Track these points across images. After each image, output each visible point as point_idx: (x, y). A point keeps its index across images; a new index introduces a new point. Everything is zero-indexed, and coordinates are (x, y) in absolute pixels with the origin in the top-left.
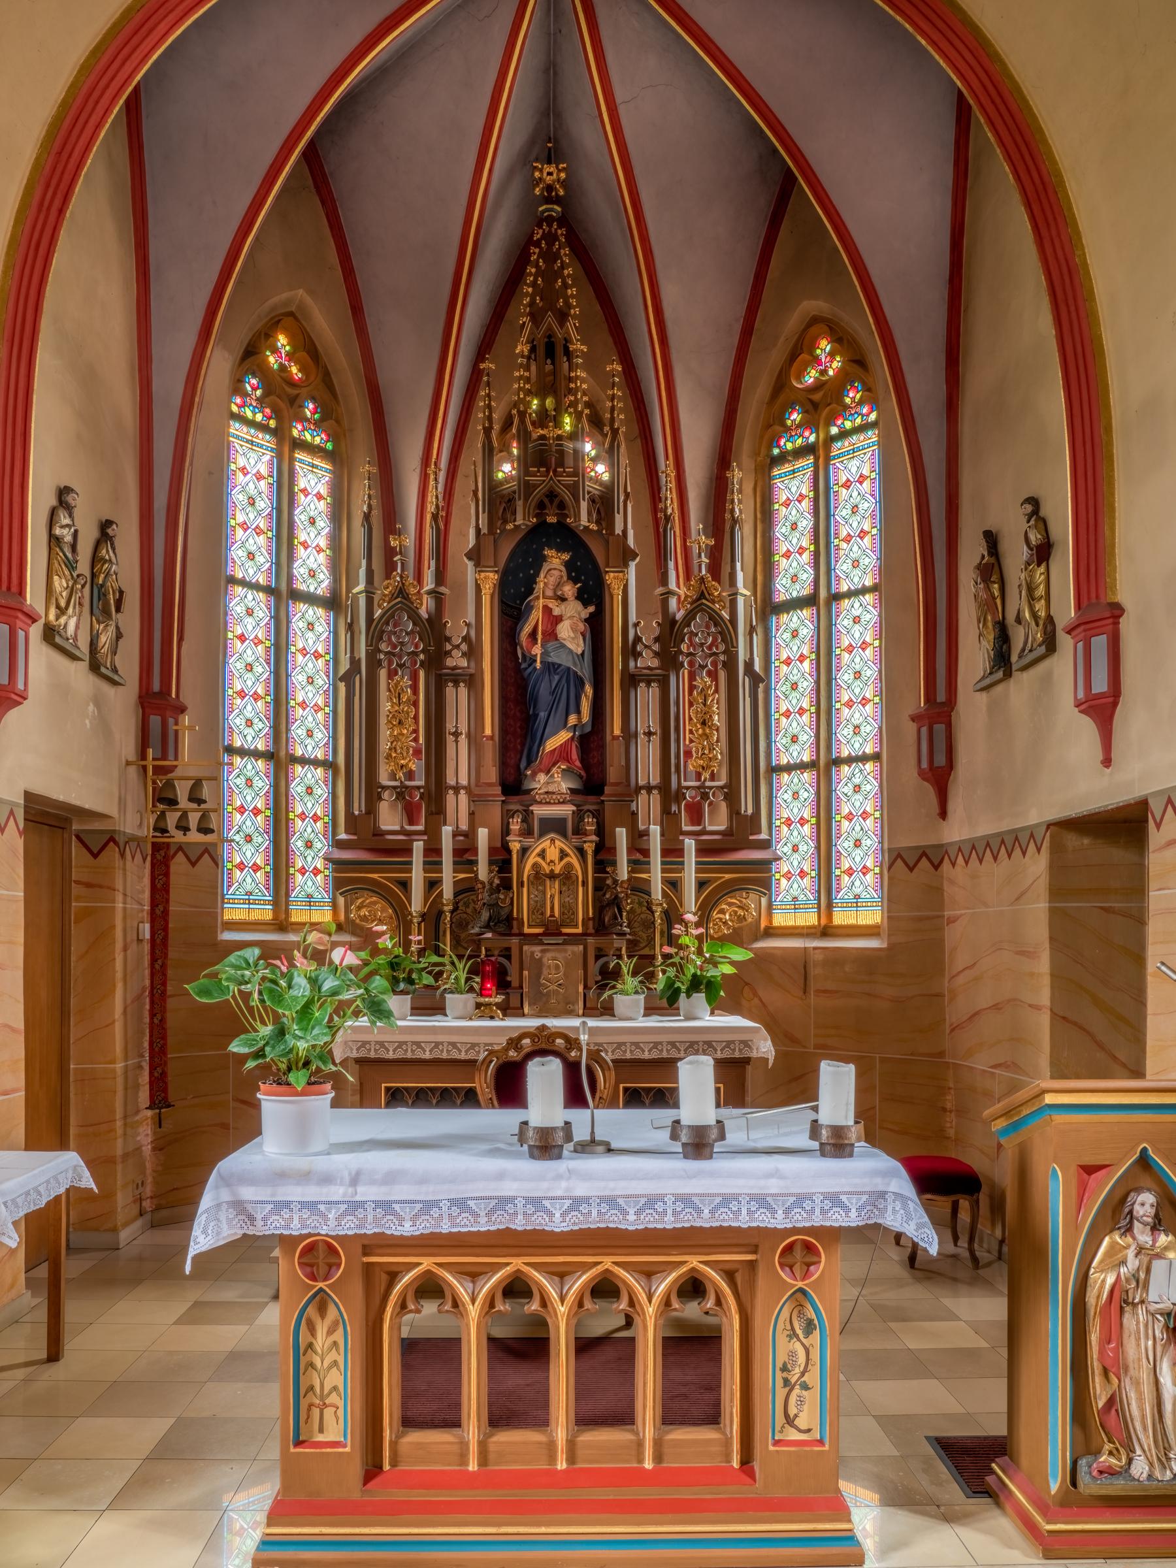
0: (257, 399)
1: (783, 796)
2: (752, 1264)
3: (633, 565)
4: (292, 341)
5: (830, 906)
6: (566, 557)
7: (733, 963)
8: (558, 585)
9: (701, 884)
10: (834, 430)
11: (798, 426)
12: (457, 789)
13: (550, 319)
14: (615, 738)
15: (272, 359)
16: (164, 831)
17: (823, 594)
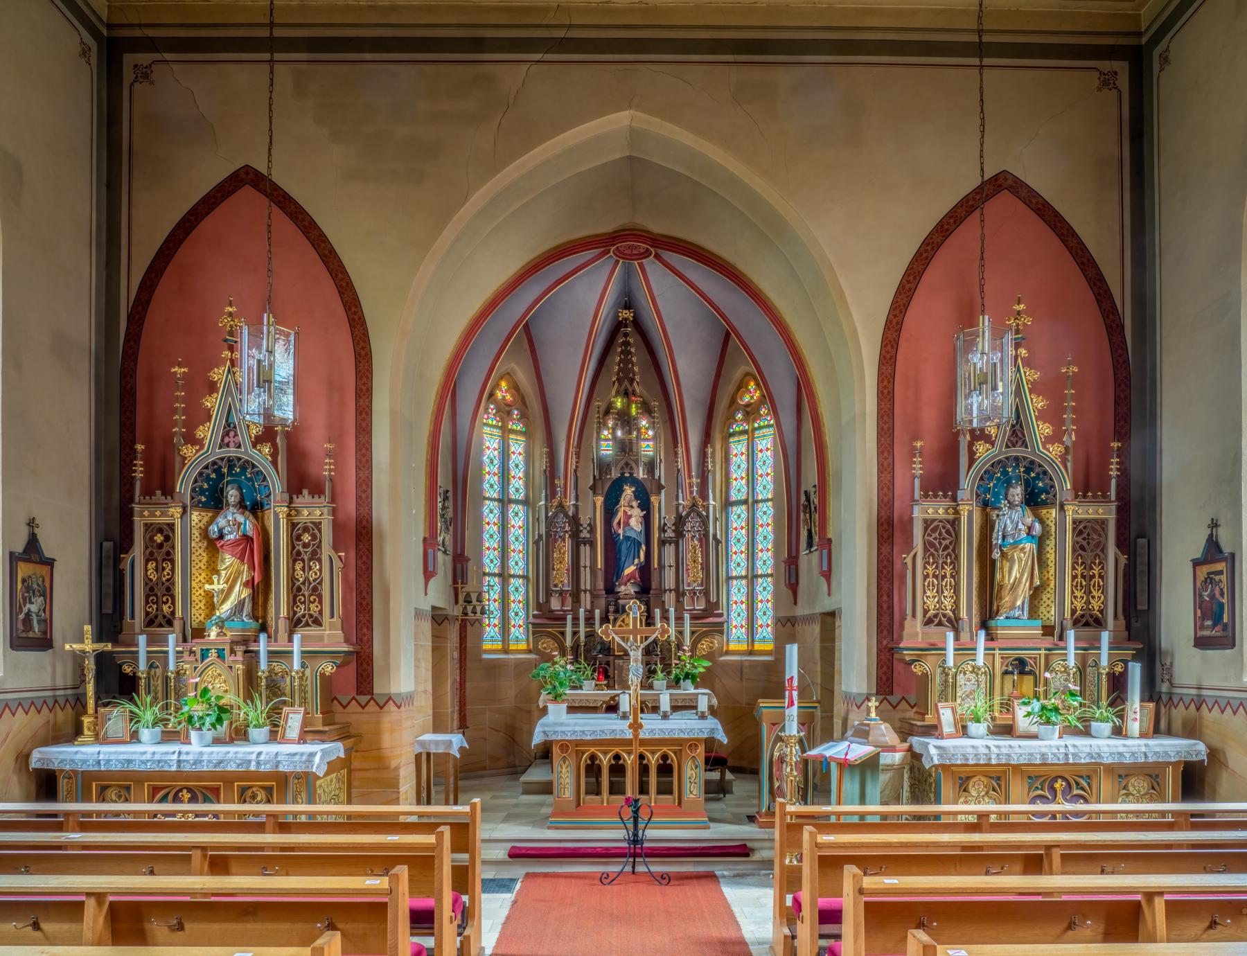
0: (494, 415)
1: (734, 590)
2: (681, 750)
3: (663, 491)
4: (508, 385)
5: (753, 641)
6: (633, 489)
7: (704, 667)
8: (630, 501)
9: (693, 633)
10: (756, 425)
11: (741, 420)
12: (585, 591)
13: (626, 382)
14: (655, 569)
15: (499, 394)
16: (466, 614)
17: (750, 500)
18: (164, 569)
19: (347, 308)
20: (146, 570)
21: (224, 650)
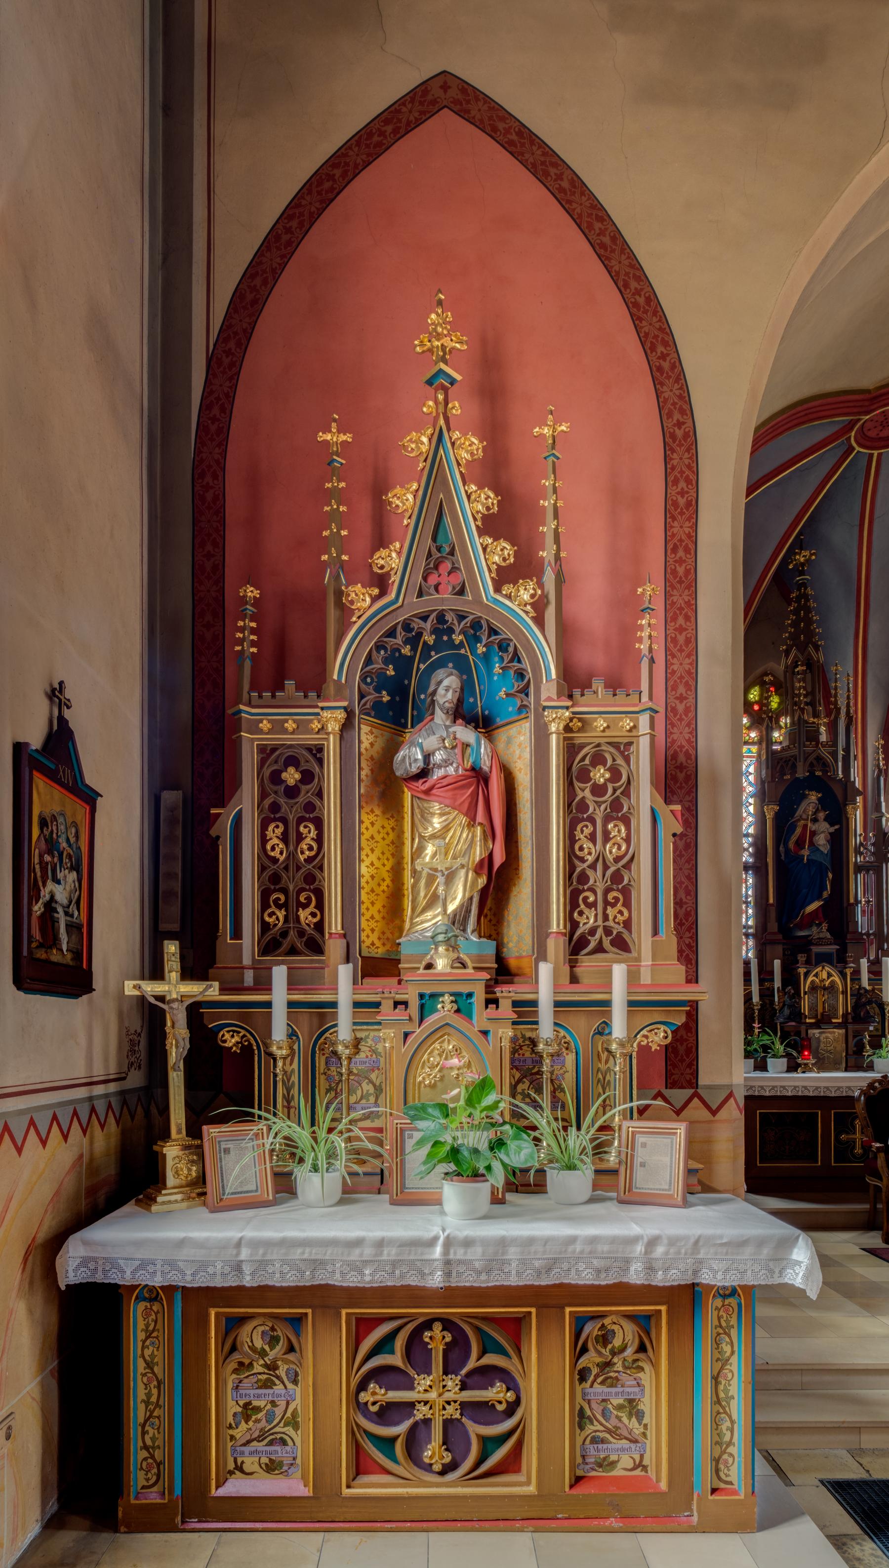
18: (300, 838)
19: (647, 348)
20: (264, 840)
21: (470, 995)
